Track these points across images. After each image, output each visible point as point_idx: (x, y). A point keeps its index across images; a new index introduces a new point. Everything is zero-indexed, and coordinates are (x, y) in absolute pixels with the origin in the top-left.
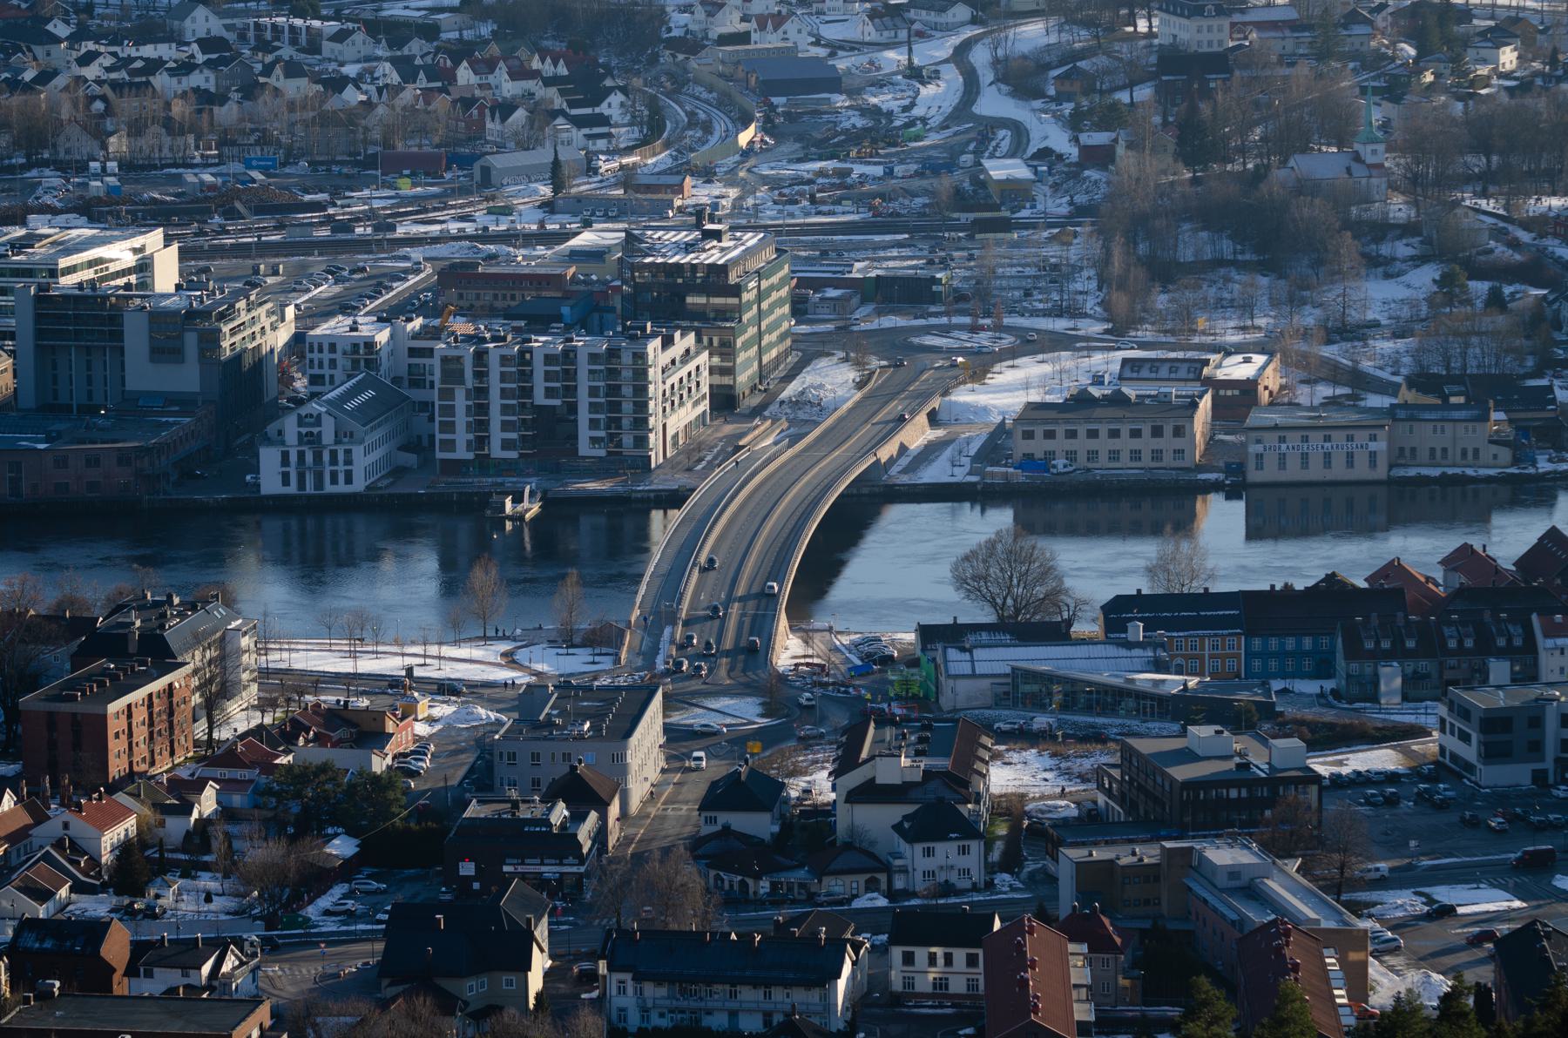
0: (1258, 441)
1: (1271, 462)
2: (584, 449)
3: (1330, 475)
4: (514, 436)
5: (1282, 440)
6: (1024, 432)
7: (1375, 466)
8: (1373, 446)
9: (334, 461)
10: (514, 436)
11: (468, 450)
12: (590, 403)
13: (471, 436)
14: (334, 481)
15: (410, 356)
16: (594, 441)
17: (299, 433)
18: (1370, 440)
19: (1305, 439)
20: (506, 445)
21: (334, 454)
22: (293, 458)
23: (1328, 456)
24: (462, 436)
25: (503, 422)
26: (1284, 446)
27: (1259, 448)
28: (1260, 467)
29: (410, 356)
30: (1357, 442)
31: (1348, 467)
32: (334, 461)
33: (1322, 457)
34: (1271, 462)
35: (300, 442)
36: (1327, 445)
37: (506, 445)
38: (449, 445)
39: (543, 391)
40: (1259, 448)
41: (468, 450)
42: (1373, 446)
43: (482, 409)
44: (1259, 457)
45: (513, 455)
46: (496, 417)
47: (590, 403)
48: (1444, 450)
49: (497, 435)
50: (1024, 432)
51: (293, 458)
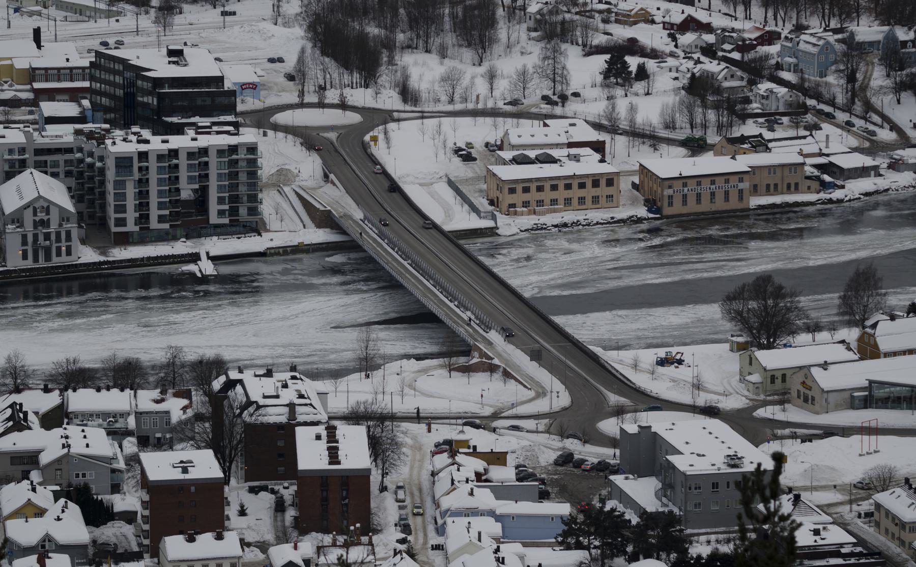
0: (670, 187)
1: (678, 201)
2: (214, 219)
3: (714, 208)
4: (167, 212)
5: (685, 185)
6: (125, 225)
7: (742, 199)
8: (741, 186)
9: (58, 239)
10: (167, 212)
11: (136, 224)
12: (218, 197)
13: (137, 215)
14: (59, 254)
15: (35, 155)
16: (221, 213)
17: (34, 221)
18: (739, 182)
19: (699, 184)
20: (161, 219)
21: (58, 234)
22: (30, 239)
23: (713, 194)
24: (131, 215)
25: (159, 203)
26: (686, 189)
27: (670, 192)
28: (671, 204)
29: (35, 155)
30: (731, 184)
31: (725, 201)
32: (58, 239)
33: (709, 194)
34: (678, 201)
35: (35, 227)
36: (713, 187)
37: (161, 219)
38: (121, 222)
39: (216, 199)
40: (670, 192)
41: (136, 224)
42: (741, 186)
43: (143, 194)
44: (670, 197)
45: (166, 226)
46: (154, 200)
47: (218, 197)
48: (776, 185)
49: (154, 213)
50: (125, 225)
51: (30, 239)
